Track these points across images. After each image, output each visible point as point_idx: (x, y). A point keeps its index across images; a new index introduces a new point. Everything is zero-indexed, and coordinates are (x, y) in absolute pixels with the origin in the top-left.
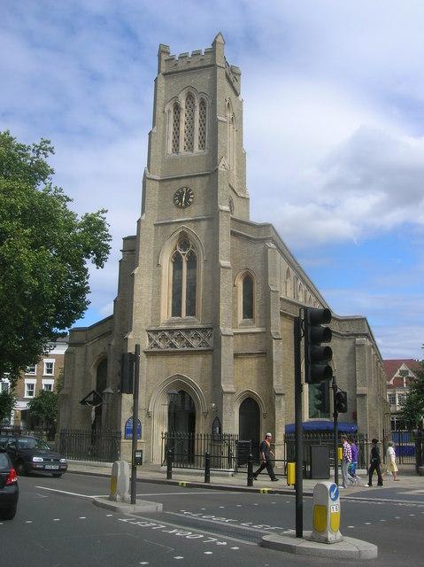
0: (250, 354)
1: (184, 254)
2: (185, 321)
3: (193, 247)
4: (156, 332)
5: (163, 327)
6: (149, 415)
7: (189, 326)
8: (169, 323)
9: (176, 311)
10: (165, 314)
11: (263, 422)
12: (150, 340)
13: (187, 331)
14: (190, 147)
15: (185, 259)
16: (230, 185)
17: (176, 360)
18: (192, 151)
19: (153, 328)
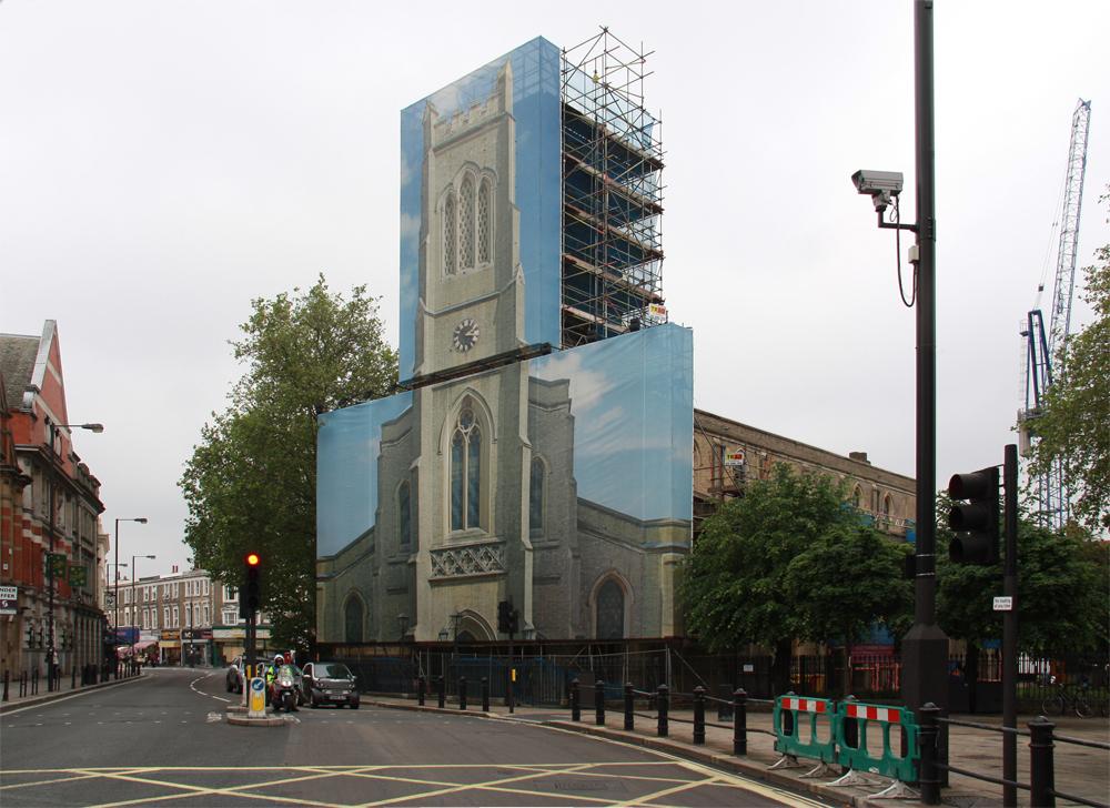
0: (540, 405)
1: (466, 434)
2: (470, 535)
3: (477, 422)
4: (439, 552)
5: (447, 544)
6: (485, 139)
7: (478, 541)
8: (454, 539)
9: (457, 524)
10: (447, 532)
11: (889, 701)
12: (434, 564)
13: (476, 547)
14: (470, 263)
15: (467, 440)
16: (84, 427)
17: (461, 589)
18: (453, 273)
19: (436, 548)
